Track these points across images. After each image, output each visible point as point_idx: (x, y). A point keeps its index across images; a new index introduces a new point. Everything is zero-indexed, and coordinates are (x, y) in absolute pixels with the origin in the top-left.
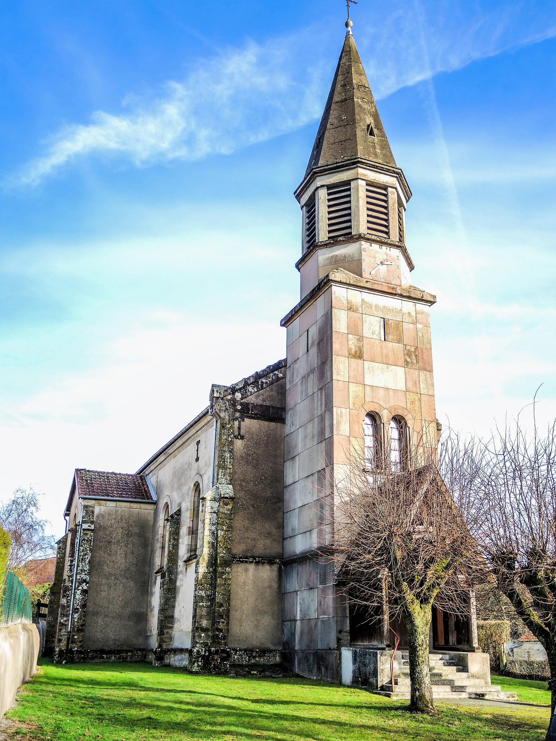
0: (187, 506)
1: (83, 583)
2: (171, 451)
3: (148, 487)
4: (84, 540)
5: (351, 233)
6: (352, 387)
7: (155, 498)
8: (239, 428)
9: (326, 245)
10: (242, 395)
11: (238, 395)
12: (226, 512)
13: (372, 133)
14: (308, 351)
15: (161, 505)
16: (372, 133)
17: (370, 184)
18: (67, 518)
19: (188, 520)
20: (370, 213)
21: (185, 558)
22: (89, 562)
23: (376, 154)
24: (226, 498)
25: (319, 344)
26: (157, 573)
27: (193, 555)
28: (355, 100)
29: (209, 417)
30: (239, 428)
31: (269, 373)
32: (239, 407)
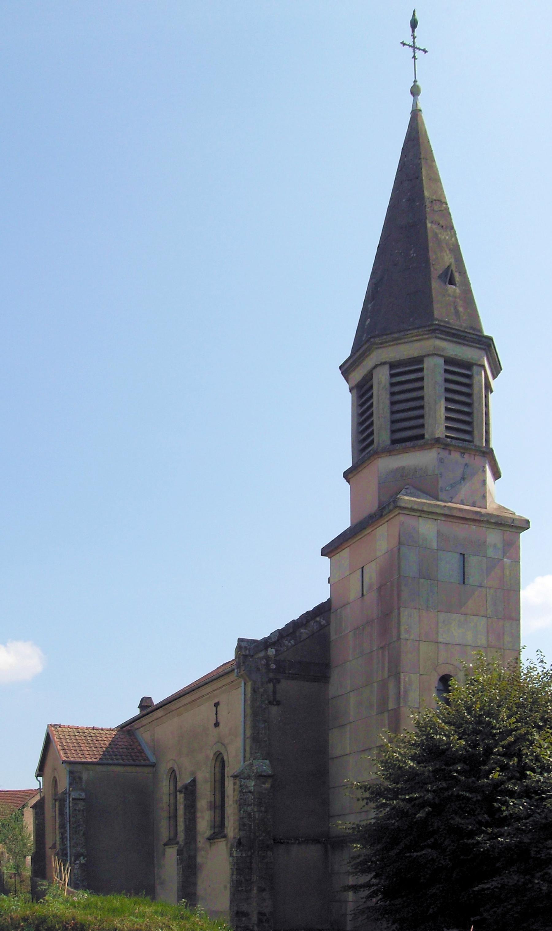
0: (205, 777)
1: (80, 856)
2: (174, 707)
3: (140, 745)
4: (75, 810)
5: (422, 436)
6: (423, 647)
7: (153, 759)
8: (274, 692)
9: (389, 451)
10: (276, 651)
11: (271, 652)
12: (264, 792)
13: (452, 282)
14: (363, 595)
15: (164, 769)
16: (452, 282)
17: (448, 361)
18: (40, 778)
19: (209, 793)
20: (450, 396)
21: (208, 834)
22: (84, 834)
23: (457, 312)
24: (265, 776)
25: (380, 589)
26: (165, 845)
27: (218, 831)
28: (429, 225)
29: (233, 676)
30: (274, 692)
31: (308, 621)
32: (273, 666)
